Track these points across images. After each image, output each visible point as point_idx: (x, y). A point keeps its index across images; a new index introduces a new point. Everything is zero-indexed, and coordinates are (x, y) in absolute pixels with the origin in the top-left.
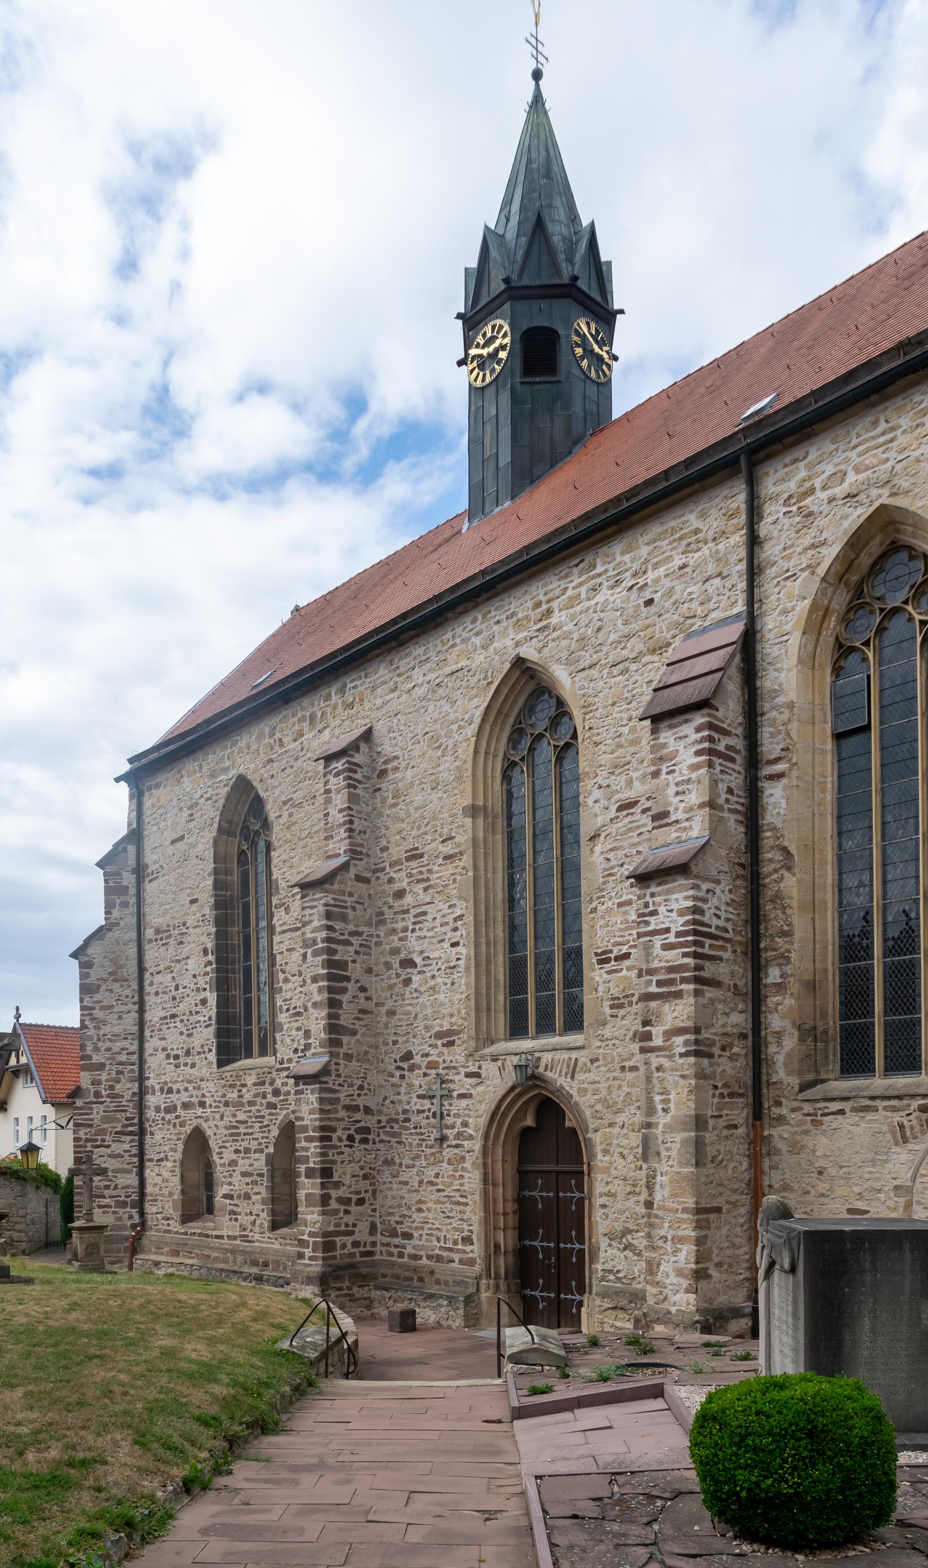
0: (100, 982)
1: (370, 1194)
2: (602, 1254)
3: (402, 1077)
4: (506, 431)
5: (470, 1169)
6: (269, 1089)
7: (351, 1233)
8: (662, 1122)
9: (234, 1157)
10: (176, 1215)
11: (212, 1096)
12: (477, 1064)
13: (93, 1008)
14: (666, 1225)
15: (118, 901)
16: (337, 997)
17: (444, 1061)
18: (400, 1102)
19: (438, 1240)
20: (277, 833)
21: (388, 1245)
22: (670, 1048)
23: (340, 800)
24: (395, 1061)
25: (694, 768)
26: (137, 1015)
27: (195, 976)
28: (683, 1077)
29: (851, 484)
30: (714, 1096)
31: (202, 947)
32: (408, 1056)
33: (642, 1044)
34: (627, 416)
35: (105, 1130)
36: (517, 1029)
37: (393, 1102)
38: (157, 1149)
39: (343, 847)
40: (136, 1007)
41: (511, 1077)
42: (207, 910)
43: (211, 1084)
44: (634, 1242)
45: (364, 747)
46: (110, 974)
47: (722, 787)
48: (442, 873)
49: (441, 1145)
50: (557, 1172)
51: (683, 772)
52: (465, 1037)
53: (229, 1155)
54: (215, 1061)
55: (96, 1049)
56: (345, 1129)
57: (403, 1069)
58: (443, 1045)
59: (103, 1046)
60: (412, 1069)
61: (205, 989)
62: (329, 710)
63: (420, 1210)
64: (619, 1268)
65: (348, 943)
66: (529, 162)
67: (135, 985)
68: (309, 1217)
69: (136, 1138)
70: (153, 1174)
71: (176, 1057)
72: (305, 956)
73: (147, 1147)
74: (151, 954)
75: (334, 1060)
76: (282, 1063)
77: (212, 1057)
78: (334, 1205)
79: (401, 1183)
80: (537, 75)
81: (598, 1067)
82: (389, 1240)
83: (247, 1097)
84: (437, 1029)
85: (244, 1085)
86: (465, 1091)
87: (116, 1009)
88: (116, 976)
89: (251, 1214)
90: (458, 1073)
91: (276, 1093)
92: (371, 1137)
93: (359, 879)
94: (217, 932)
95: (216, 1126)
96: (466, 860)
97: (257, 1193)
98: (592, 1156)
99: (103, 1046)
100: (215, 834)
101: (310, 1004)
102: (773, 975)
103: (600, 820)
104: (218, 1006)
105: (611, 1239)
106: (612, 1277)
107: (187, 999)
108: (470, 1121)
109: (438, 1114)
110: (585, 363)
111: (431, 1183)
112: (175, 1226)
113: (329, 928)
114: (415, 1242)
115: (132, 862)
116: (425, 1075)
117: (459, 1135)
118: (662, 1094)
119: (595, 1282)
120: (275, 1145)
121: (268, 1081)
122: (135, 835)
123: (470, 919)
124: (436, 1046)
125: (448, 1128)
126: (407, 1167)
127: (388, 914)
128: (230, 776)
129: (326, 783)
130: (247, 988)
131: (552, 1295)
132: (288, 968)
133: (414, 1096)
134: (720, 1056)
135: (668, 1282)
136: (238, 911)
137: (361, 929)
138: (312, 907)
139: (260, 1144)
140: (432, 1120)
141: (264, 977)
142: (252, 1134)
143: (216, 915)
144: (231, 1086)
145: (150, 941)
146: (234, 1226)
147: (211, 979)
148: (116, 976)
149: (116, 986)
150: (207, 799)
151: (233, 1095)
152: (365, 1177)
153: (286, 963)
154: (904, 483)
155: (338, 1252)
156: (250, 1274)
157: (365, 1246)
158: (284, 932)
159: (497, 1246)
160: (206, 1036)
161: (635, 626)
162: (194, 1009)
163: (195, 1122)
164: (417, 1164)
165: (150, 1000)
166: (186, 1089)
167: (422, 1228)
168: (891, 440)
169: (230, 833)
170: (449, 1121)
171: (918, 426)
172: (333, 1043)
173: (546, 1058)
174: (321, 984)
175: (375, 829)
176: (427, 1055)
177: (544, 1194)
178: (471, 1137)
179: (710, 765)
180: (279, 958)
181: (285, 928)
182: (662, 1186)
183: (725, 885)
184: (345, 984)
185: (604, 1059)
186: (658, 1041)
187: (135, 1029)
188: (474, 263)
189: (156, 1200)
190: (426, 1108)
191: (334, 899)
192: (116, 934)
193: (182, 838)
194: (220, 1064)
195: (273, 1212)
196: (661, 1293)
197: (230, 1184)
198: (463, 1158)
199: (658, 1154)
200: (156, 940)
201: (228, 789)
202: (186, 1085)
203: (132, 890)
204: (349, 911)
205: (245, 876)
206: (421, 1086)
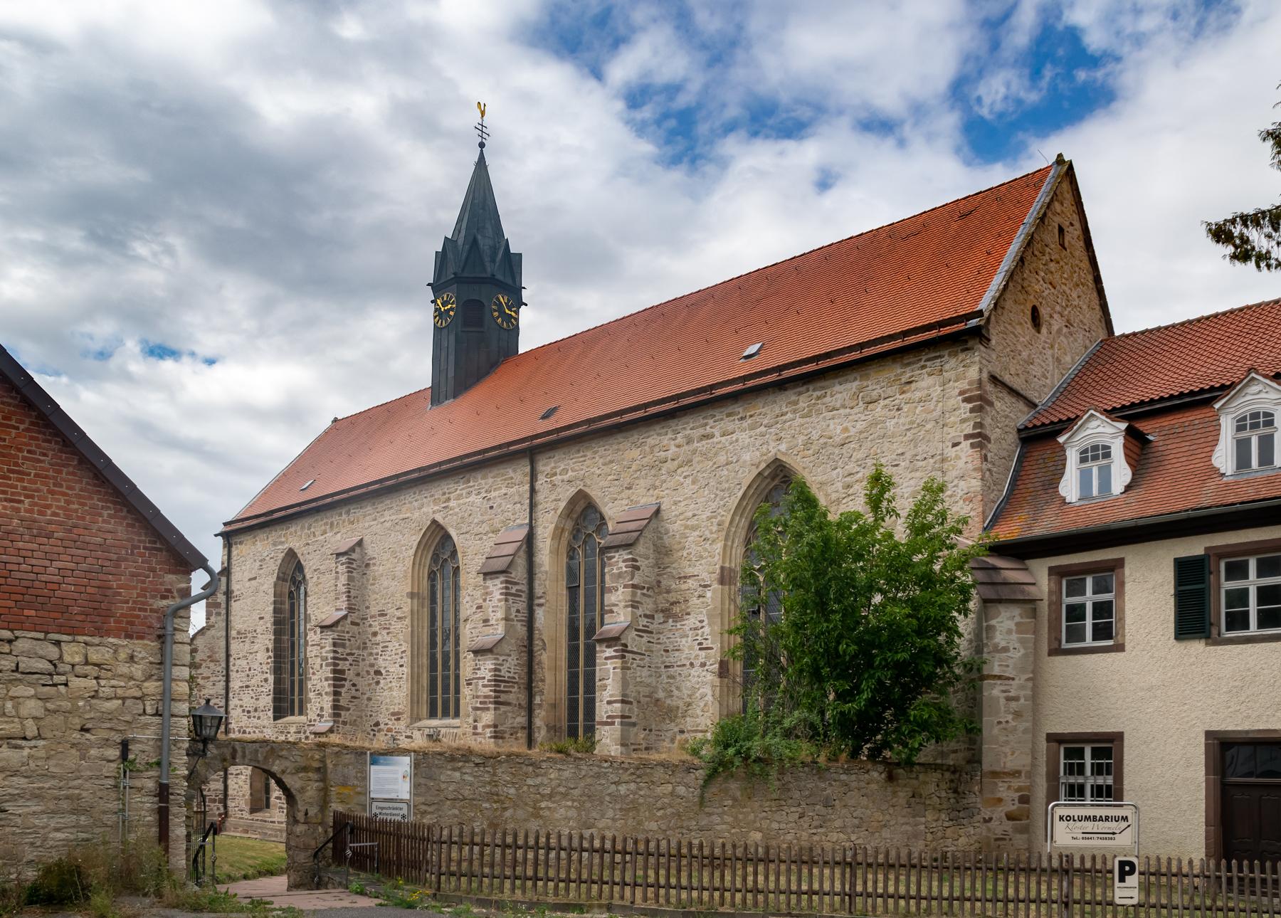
10: (247, 808)
23: (343, 579)
25: (500, 600)
32: (377, 724)
36: (433, 714)
39: (345, 605)
42: (269, 625)
45: (358, 549)
47: (513, 610)
48: (396, 626)
51: (495, 602)
60: (379, 731)
65: (346, 659)
66: (474, 198)
67: (224, 665)
74: (234, 646)
77: (271, 714)
80: (482, 145)
88: (211, 658)
93: (353, 623)
96: (407, 622)
102: (537, 700)
103: (469, 612)
112: (246, 815)
113: (335, 652)
115: (223, 588)
123: (409, 653)
127: (369, 644)
136: (288, 627)
148: (211, 658)
149: (212, 665)
160: (267, 701)
161: (486, 518)
165: (233, 675)
169: (284, 580)
172: (336, 715)
173: (443, 731)
175: (363, 595)
179: (506, 600)
183: (514, 656)
186: (480, 730)
192: (212, 632)
194: (275, 718)
203: (223, 605)
205: (292, 605)
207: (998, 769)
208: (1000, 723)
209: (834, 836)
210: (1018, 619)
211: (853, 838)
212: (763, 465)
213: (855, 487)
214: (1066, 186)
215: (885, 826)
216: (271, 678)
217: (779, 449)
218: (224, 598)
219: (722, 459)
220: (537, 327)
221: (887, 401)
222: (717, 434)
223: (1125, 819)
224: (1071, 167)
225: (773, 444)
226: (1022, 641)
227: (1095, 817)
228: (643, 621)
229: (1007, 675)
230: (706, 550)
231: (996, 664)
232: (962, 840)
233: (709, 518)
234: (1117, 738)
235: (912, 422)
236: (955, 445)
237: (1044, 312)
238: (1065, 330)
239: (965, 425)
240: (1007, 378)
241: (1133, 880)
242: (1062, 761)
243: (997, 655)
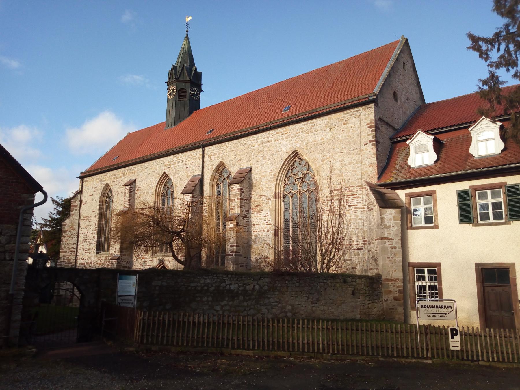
4: (174, 111)
20: (115, 199)
23: (127, 195)
42: (97, 214)
45: (134, 184)
55: (65, 247)
59: (67, 246)
67: (77, 231)
74: (82, 223)
77: (95, 251)
80: (187, 32)
83: (102, 262)
88: (72, 228)
99: (67, 246)
115: (79, 199)
122: (80, 192)
149: (72, 231)
151: (99, 262)
154: (224, 158)
160: (94, 246)
187: (76, 242)
194: (97, 253)
203: (79, 206)
207: (389, 278)
208: (389, 258)
209: (322, 308)
210: (394, 214)
211: (330, 308)
212: (291, 153)
213: (326, 161)
214: (405, 47)
215: (343, 303)
216: (96, 236)
217: (297, 147)
218: (79, 203)
219: (275, 150)
220: (206, 100)
221: (338, 128)
222: (273, 140)
223: (450, 307)
224: (407, 40)
225: (294, 144)
226: (396, 224)
227: (437, 306)
228: (245, 213)
229: (391, 237)
230: (269, 185)
231: (386, 233)
232: (376, 309)
233: (270, 173)
234: (439, 265)
235: (348, 136)
236: (365, 144)
237: (399, 94)
238: (406, 101)
239: (369, 137)
240: (385, 119)
241: (457, 338)
242: (416, 275)
243: (386, 229)
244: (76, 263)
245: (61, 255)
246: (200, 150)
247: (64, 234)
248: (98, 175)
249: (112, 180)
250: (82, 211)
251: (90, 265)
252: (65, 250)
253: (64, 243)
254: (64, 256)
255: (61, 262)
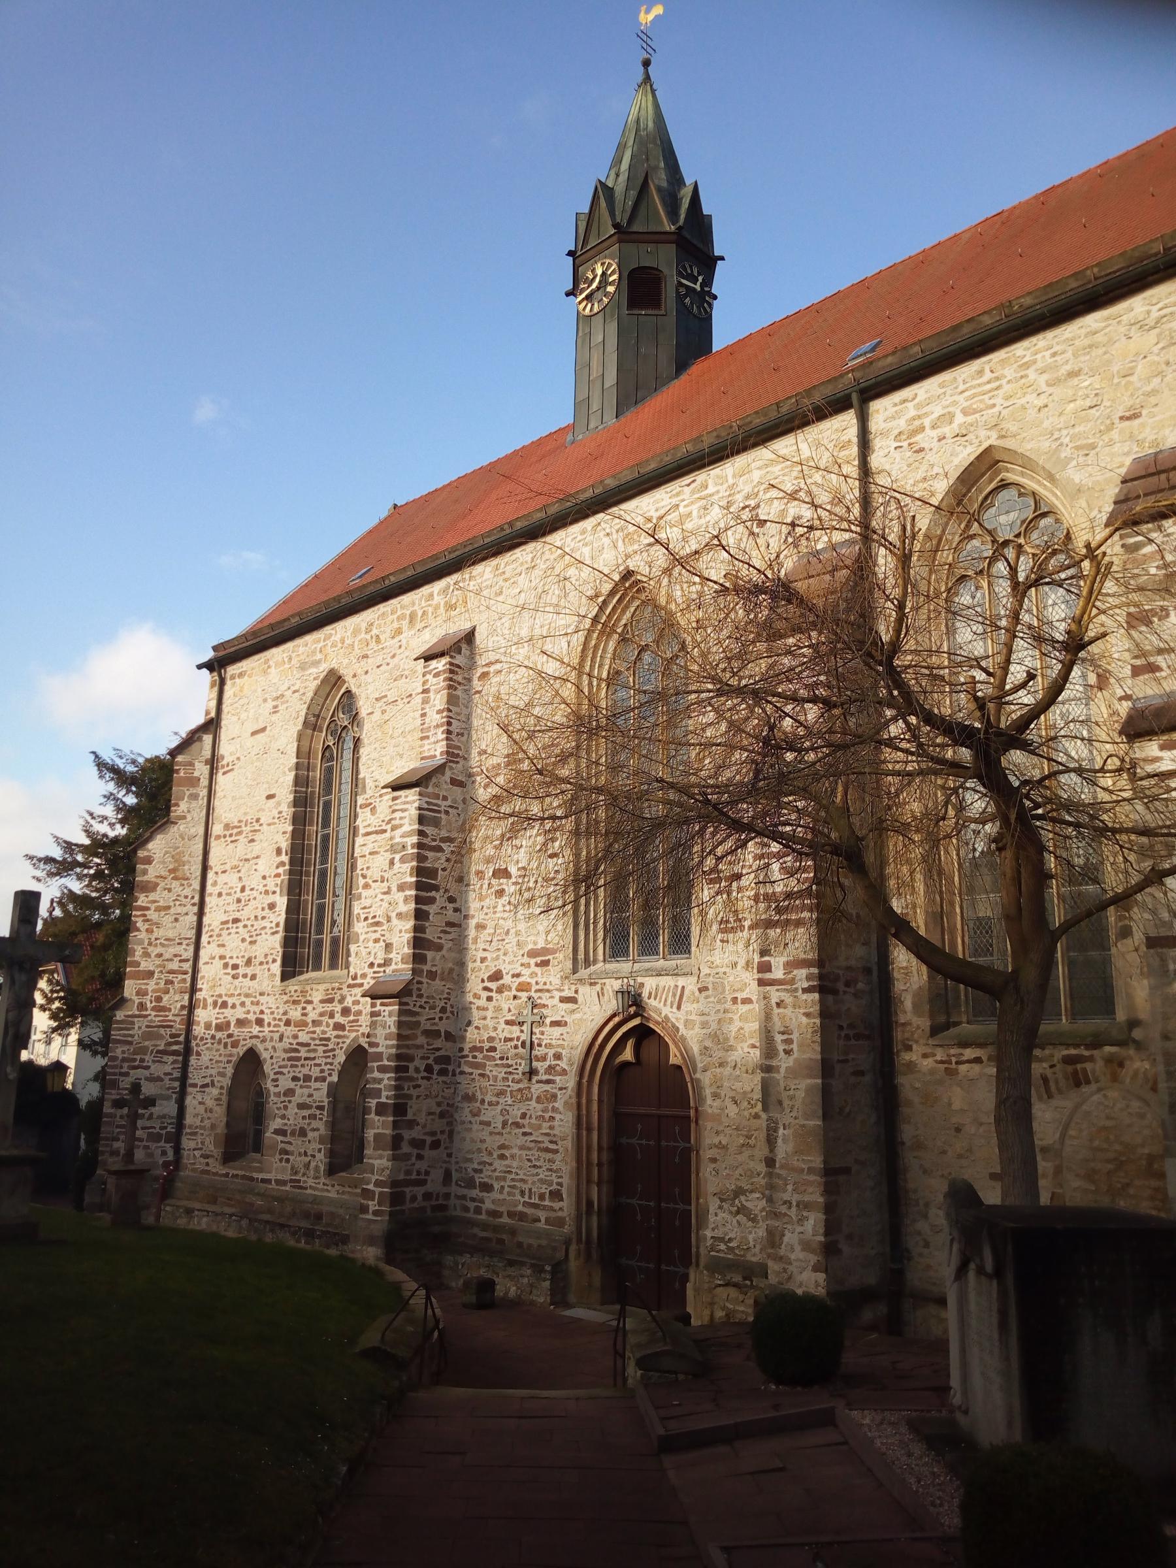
0: (158, 881)
1: (445, 1136)
2: (712, 1218)
3: (489, 999)
5: (561, 1109)
6: (338, 1008)
7: (422, 1183)
8: (784, 1066)
9: (292, 1085)
10: (217, 1152)
11: (272, 1013)
12: (573, 988)
13: (148, 909)
14: (790, 1188)
15: (187, 793)
16: (424, 907)
17: (537, 983)
18: (486, 1027)
19: (522, 1193)
21: (464, 1197)
22: (792, 981)
23: (439, 700)
24: (483, 981)
26: (195, 918)
27: (264, 878)
28: (807, 1015)
29: (960, 426)
30: (839, 1037)
31: (276, 846)
32: (497, 976)
33: (760, 975)
34: (731, 350)
35: (147, 1048)
36: (618, 950)
37: (477, 1028)
38: (203, 1073)
40: (196, 909)
41: (611, 1004)
43: (271, 999)
44: (748, 1205)
46: (170, 871)
49: (530, 1080)
50: (659, 1116)
52: (561, 956)
53: (285, 1083)
54: (278, 973)
55: (146, 955)
56: (423, 1058)
57: (490, 990)
58: (537, 965)
59: (153, 951)
60: (500, 990)
61: (274, 892)
62: (430, 609)
63: (502, 1157)
64: (731, 1235)
65: (439, 849)
67: (196, 885)
68: (377, 1163)
69: (180, 1058)
70: (195, 1102)
71: (235, 967)
72: (392, 863)
73: (191, 1069)
75: (417, 978)
76: (355, 978)
77: (276, 968)
78: (406, 1148)
79: (481, 1123)
80: (646, 63)
81: (707, 997)
82: (465, 1191)
83: (313, 1015)
84: (530, 946)
85: (310, 1002)
86: (559, 1018)
87: (172, 911)
88: (175, 873)
89: (306, 1154)
90: (552, 997)
91: (346, 1012)
92: (450, 1068)
93: (454, 782)
94: (293, 831)
95: (274, 1048)
97: (314, 1130)
98: (700, 1099)
99: (153, 951)
100: (300, 727)
101: (393, 915)
104: (287, 912)
105: (722, 1200)
106: (723, 1247)
107: (252, 902)
108: (564, 1053)
109: (528, 1043)
110: (687, 300)
111: (517, 1125)
112: (216, 1167)
114: (495, 1195)
115: (207, 753)
116: (515, 997)
117: (550, 1069)
118: (783, 1033)
119: (702, 1251)
120: (340, 1073)
121: (337, 997)
122: (212, 725)
124: (529, 965)
125: (538, 1060)
126: (490, 1104)
128: (321, 669)
129: (424, 683)
130: (322, 894)
131: (651, 1266)
132: (369, 873)
133: (502, 1021)
134: (845, 992)
135: (793, 1257)
137: (454, 835)
138: (403, 810)
139: (322, 1071)
140: (521, 1050)
141: (340, 881)
142: (314, 1058)
143: (294, 813)
144: (295, 1002)
145: (218, 837)
146: (284, 1169)
147: (282, 882)
149: (175, 884)
150: (295, 692)
151: (295, 1014)
152: (442, 1115)
153: (368, 868)
154: (1012, 427)
155: (408, 1205)
156: (300, 1228)
157: (437, 1199)
158: (368, 834)
159: (590, 1203)
160: (272, 944)
162: (260, 914)
163: (249, 1043)
164: (501, 1101)
166: (243, 1004)
167: (504, 1179)
168: (997, 389)
170: (538, 1051)
171: (1022, 377)
172: (418, 959)
174: (408, 893)
176: (518, 975)
177: (644, 1142)
178: (564, 1072)
180: (360, 864)
181: (369, 830)
182: (785, 1141)
184: (433, 894)
185: (715, 989)
186: (778, 973)
187: (192, 934)
188: (586, 209)
189: (195, 1134)
190: (515, 1035)
191: (427, 802)
193: (263, 730)
194: (285, 977)
195: (331, 1154)
196: (785, 1270)
197: (283, 1117)
198: (554, 1096)
199: (780, 1103)
200: (225, 836)
201: (318, 682)
202: (243, 999)
203: (204, 782)
204: (443, 816)
206: (510, 1010)
216: (282, 902)
244: (189, 1022)
245: (130, 988)
246: (846, 422)
247: (142, 900)
248: (289, 645)
249: (357, 652)
250: (217, 803)
251: (256, 1030)
252: (145, 965)
253: (142, 935)
254: (141, 993)
255: (129, 1022)
